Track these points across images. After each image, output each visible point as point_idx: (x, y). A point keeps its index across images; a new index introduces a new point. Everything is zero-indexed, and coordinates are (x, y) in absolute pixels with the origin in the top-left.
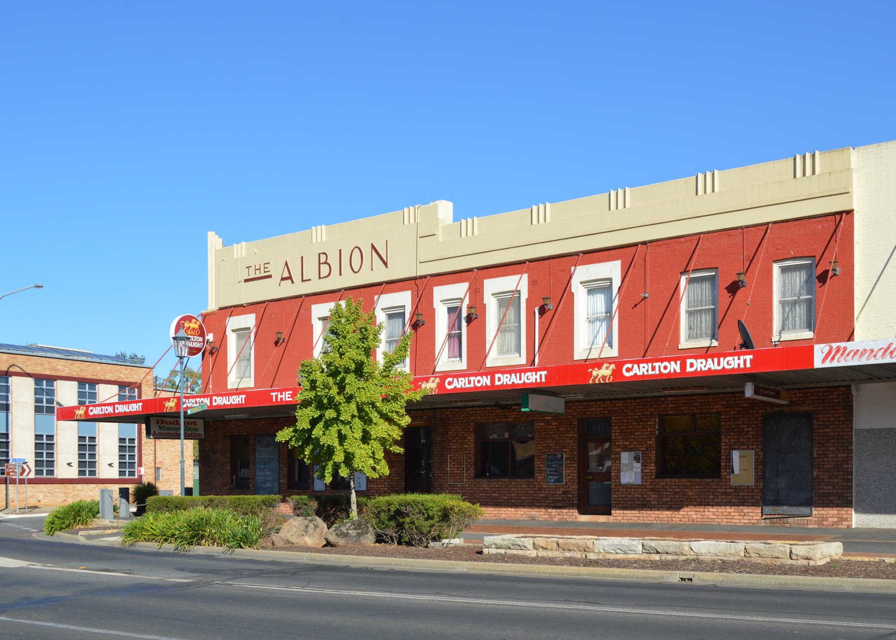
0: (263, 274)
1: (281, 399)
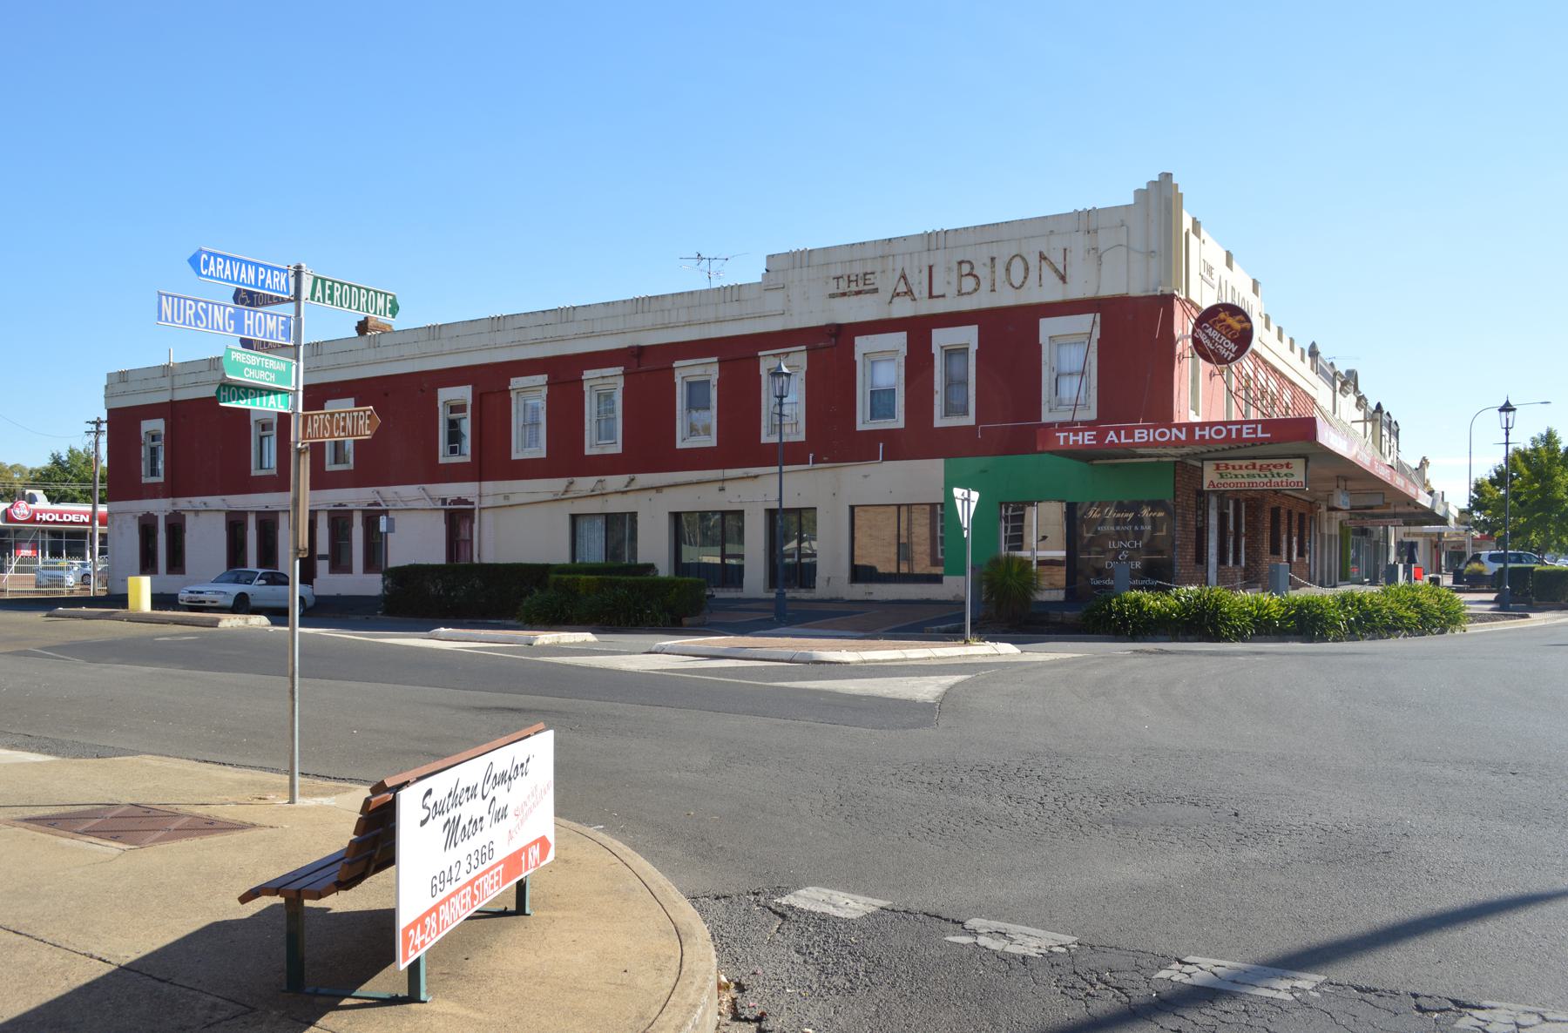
0: (861, 287)
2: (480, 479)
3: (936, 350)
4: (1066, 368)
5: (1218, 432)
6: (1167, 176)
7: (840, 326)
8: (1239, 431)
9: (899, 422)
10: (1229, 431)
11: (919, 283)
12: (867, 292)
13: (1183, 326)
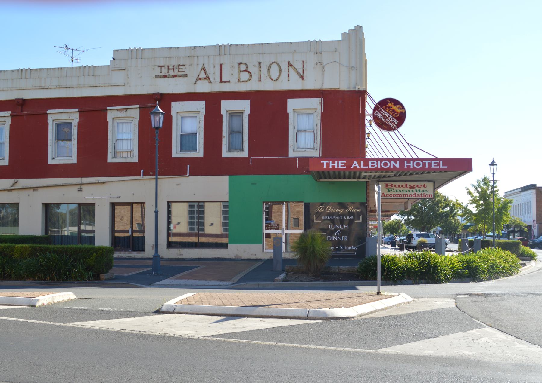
0: (176, 73)
3: (223, 112)
4: (302, 127)
5: (418, 164)
6: (359, 28)
7: (162, 95)
8: (430, 164)
9: (200, 153)
10: (424, 164)
11: (214, 74)
12: (181, 76)
13: (369, 109)
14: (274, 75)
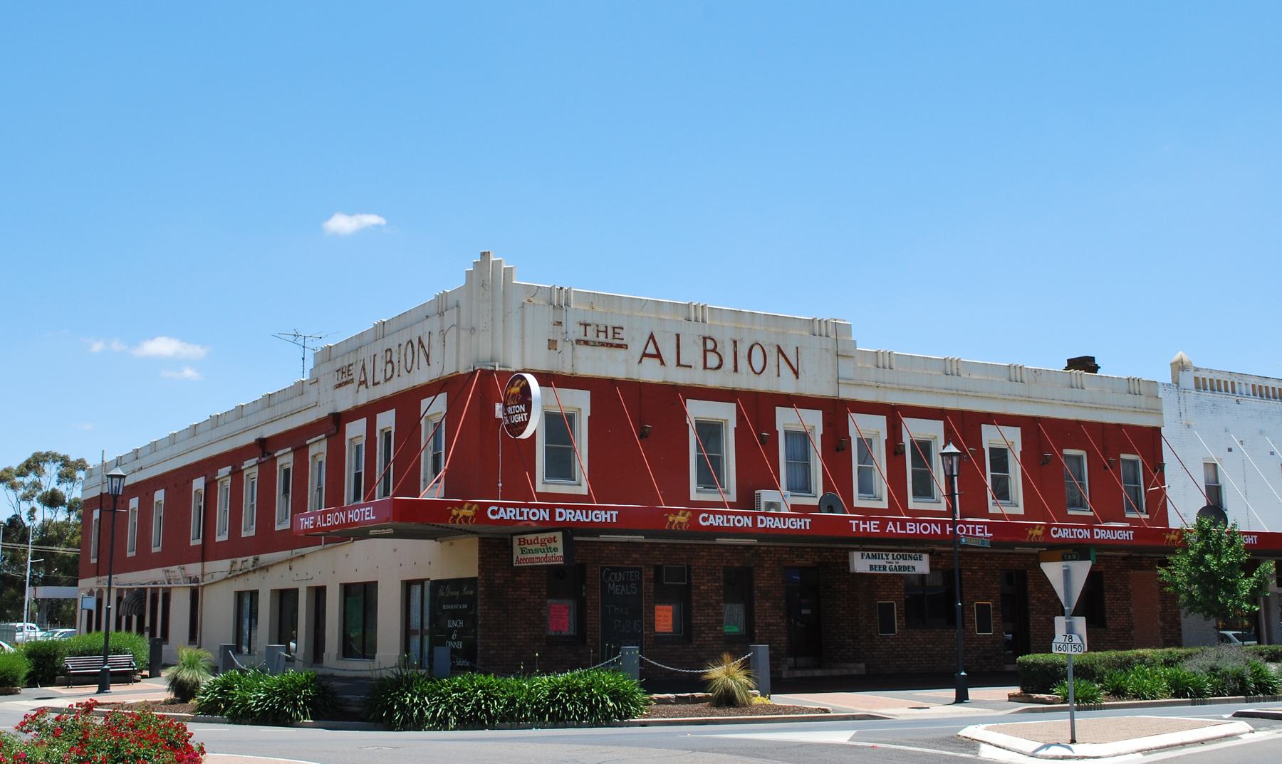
0: (610, 340)
1: (865, 529)
2: (203, 561)
11: (668, 352)
14: (758, 361)
